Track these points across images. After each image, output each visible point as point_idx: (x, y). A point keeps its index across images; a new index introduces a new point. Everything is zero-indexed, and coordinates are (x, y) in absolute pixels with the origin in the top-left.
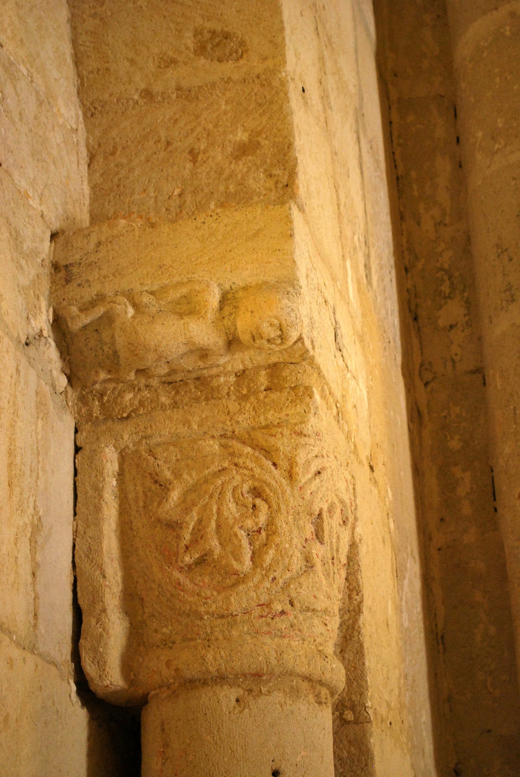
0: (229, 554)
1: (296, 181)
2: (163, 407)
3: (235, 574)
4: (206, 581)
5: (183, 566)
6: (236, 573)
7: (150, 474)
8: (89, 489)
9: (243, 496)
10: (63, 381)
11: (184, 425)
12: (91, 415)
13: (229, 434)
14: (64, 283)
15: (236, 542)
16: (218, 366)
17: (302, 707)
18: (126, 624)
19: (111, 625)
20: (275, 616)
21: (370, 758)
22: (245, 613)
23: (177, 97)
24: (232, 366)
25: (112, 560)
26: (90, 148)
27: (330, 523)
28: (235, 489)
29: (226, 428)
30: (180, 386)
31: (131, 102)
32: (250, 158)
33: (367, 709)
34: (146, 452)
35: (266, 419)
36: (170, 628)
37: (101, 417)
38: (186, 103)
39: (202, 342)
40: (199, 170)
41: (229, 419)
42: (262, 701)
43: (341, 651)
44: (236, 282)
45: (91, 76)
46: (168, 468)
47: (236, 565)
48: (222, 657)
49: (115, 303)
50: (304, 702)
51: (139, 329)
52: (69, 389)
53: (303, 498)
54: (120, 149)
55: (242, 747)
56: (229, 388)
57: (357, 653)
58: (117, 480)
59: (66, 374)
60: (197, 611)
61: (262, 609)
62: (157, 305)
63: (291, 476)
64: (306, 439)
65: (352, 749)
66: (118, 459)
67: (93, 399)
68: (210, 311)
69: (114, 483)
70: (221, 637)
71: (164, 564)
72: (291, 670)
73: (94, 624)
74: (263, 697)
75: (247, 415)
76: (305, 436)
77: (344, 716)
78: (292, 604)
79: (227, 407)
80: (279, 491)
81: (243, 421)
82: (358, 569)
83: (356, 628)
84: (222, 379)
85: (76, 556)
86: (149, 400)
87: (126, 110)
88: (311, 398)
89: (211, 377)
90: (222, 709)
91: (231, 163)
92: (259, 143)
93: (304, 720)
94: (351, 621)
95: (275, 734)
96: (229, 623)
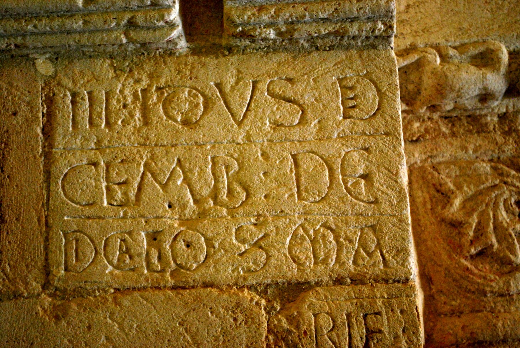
0: (505, 249)
2: (444, 134)
3: (509, 264)
4: (487, 268)
7: (434, 185)
9: (512, 206)
11: (462, 150)
13: (495, 160)
15: (510, 240)
28: (505, 201)
30: (455, 120)
39: (493, 89)
48: (508, 326)
49: (426, 52)
51: (448, 74)
56: (494, 126)
60: (484, 289)
62: (459, 58)
68: (502, 65)
70: (502, 310)
71: (452, 253)
75: (511, 147)
81: (508, 151)
84: (489, 118)
86: (433, 129)
89: (481, 116)
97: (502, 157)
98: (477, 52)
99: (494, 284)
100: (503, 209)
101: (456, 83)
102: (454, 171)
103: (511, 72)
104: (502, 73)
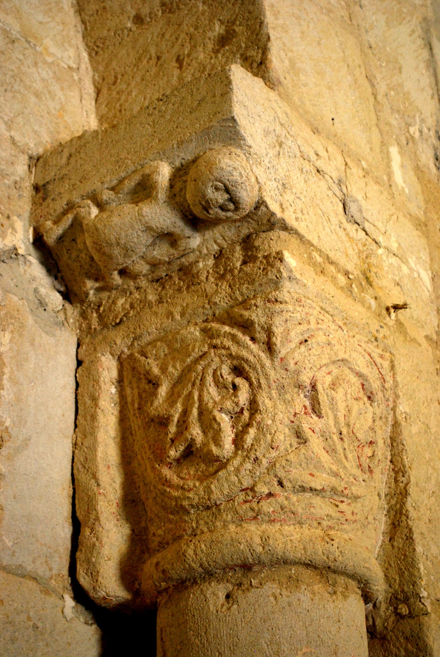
0: (210, 440)
1: (269, 56)
3: (216, 461)
4: (192, 473)
5: (170, 461)
6: (217, 459)
8: (87, 400)
10: (56, 299)
12: (90, 328)
13: (210, 318)
14: (41, 201)
15: (216, 426)
16: (193, 251)
17: (303, 598)
18: (126, 530)
19: (105, 533)
20: (260, 499)
21: (428, 654)
22: (228, 501)
23: (163, 13)
24: (207, 248)
25: (109, 467)
26: (96, 84)
27: (329, 394)
28: (215, 371)
29: (206, 312)
31: (126, 32)
32: (227, 48)
33: (422, 600)
34: (138, 353)
35: (242, 294)
36: (163, 529)
37: (98, 328)
38: (171, 15)
39: (158, 225)
40: (184, 75)
41: (207, 301)
42: (252, 595)
43: (390, 539)
44: (185, 157)
45: (92, 18)
46: (157, 365)
47: (215, 450)
50: (306, 592)
52: (67, 305)
53: (286, 370)
54: (119, 77)
55: (230, 648)
56: (208, 272)
57: (407, 539)
58: (116, 388)
59: (59, 292)
61: (247, 494)
63: (270, 348)
64: (282, 306)
65: (409, 646)
66: (117, 366)
67: (92, 312)
68: (160, 190)
69: (113, 390)
70: (205, 530)
72: (281, 556)
73: (89, 534)
74: (253, 590)
76: (281, 303)
77: (399, 611)
78: (281, 484)
79: (205, 290)
80: (258, 366)
81: (220, 301)
82: (403, 449)
83: (404, 512)
84: (201, 265)
85: (75, 468)
86: (138, 302)
87: (122, 40)
88: (281, 261)
89: (191, 264)
90: (209, 608)
91: (211, 58)
92: (234, 31)
93: (305, 612)
94: (398, 506)
95: (268, 630)
96: (213, 513)
97: (217, 312)
98: (133, 184)
99: (191, 495)
100: (212, 384)
101: (110, 235)
102: (162, 350)
103: (175, 195)
104: (162, 201)
